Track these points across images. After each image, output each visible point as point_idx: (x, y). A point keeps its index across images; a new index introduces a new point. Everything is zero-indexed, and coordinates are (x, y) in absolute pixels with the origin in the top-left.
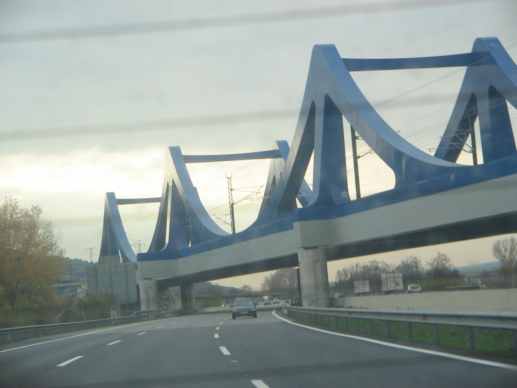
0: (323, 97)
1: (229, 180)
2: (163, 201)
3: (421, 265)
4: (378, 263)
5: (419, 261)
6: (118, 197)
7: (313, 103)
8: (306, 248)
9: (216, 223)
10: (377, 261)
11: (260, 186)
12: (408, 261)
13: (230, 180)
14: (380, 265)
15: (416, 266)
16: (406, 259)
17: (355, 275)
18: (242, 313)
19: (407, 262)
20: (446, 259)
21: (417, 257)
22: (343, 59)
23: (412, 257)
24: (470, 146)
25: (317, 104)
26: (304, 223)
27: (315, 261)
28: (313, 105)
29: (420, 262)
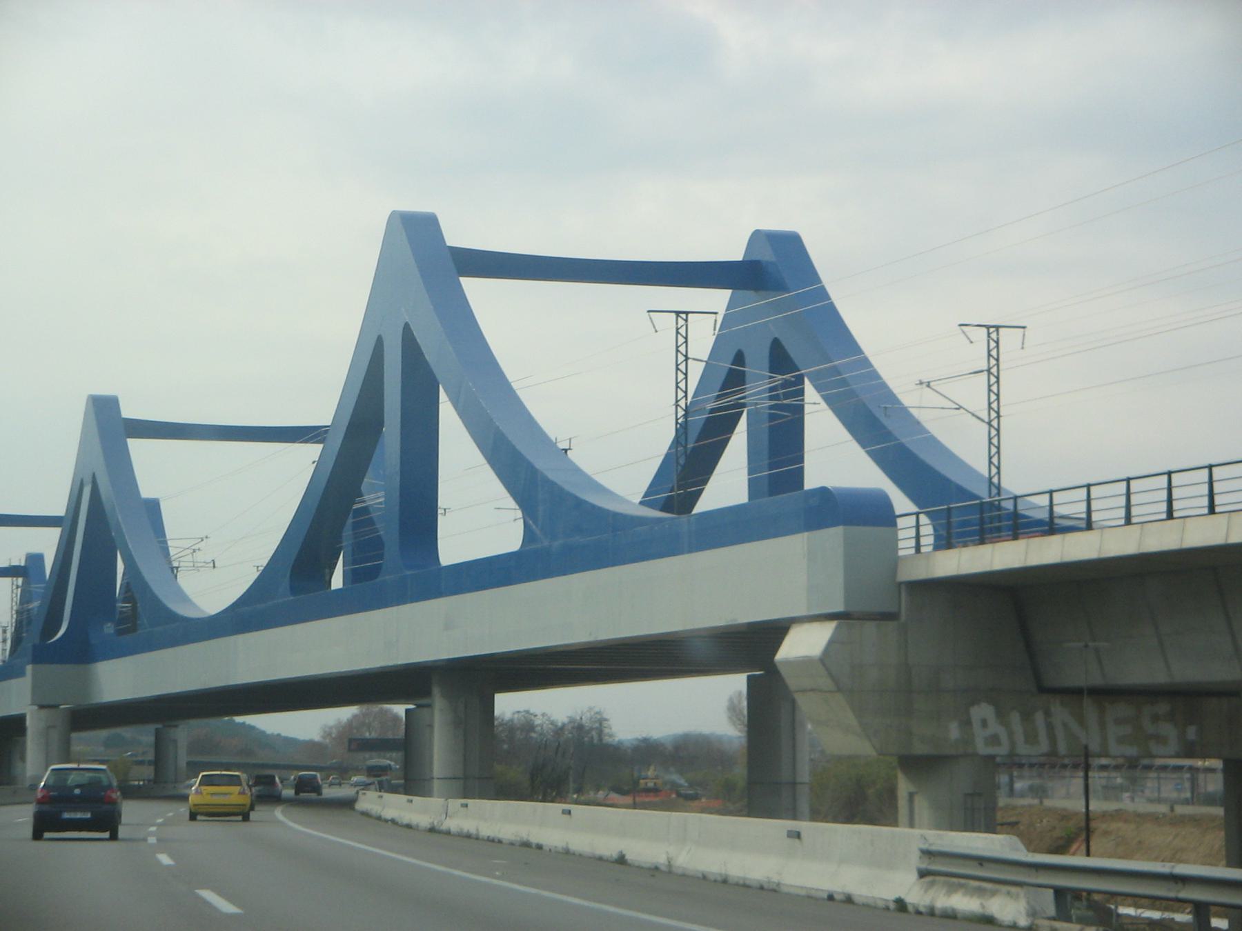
0: (403, 325)
1: (681, 322)
2: (65, 523)
3: (611, 729)
4: (536, 716)
5: (606, 720)
6: (128, 411)
7: (379, 343)
8: (42, 707)
9: (914, 412)
10: (532, 711)
11: (199, 538)
12: (583, 717)
13: (686, 320)
14: (538, 722)
15: (600, 732)
16: (580, 712)
17: (546, 742)
18: (240, 818)
19: (581, 718)
20: (601, 721)
21: (602, 710)
22: (449, 247)
23: (590, 709)
24: (950, 407)
25: (85, 480)
26: (847, 527)
27: (49, 727)
28: (379, 343)
29: (609, 723)
